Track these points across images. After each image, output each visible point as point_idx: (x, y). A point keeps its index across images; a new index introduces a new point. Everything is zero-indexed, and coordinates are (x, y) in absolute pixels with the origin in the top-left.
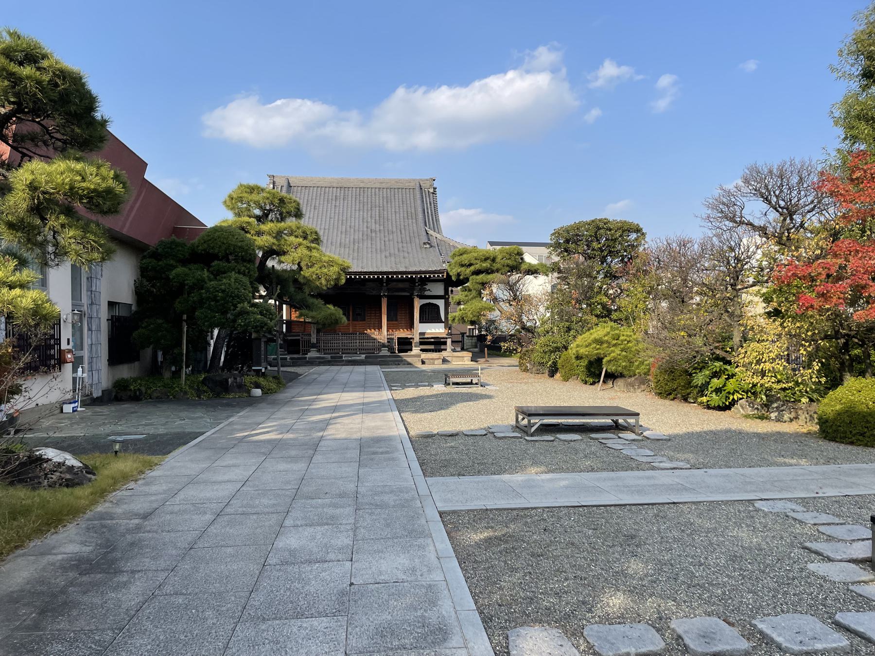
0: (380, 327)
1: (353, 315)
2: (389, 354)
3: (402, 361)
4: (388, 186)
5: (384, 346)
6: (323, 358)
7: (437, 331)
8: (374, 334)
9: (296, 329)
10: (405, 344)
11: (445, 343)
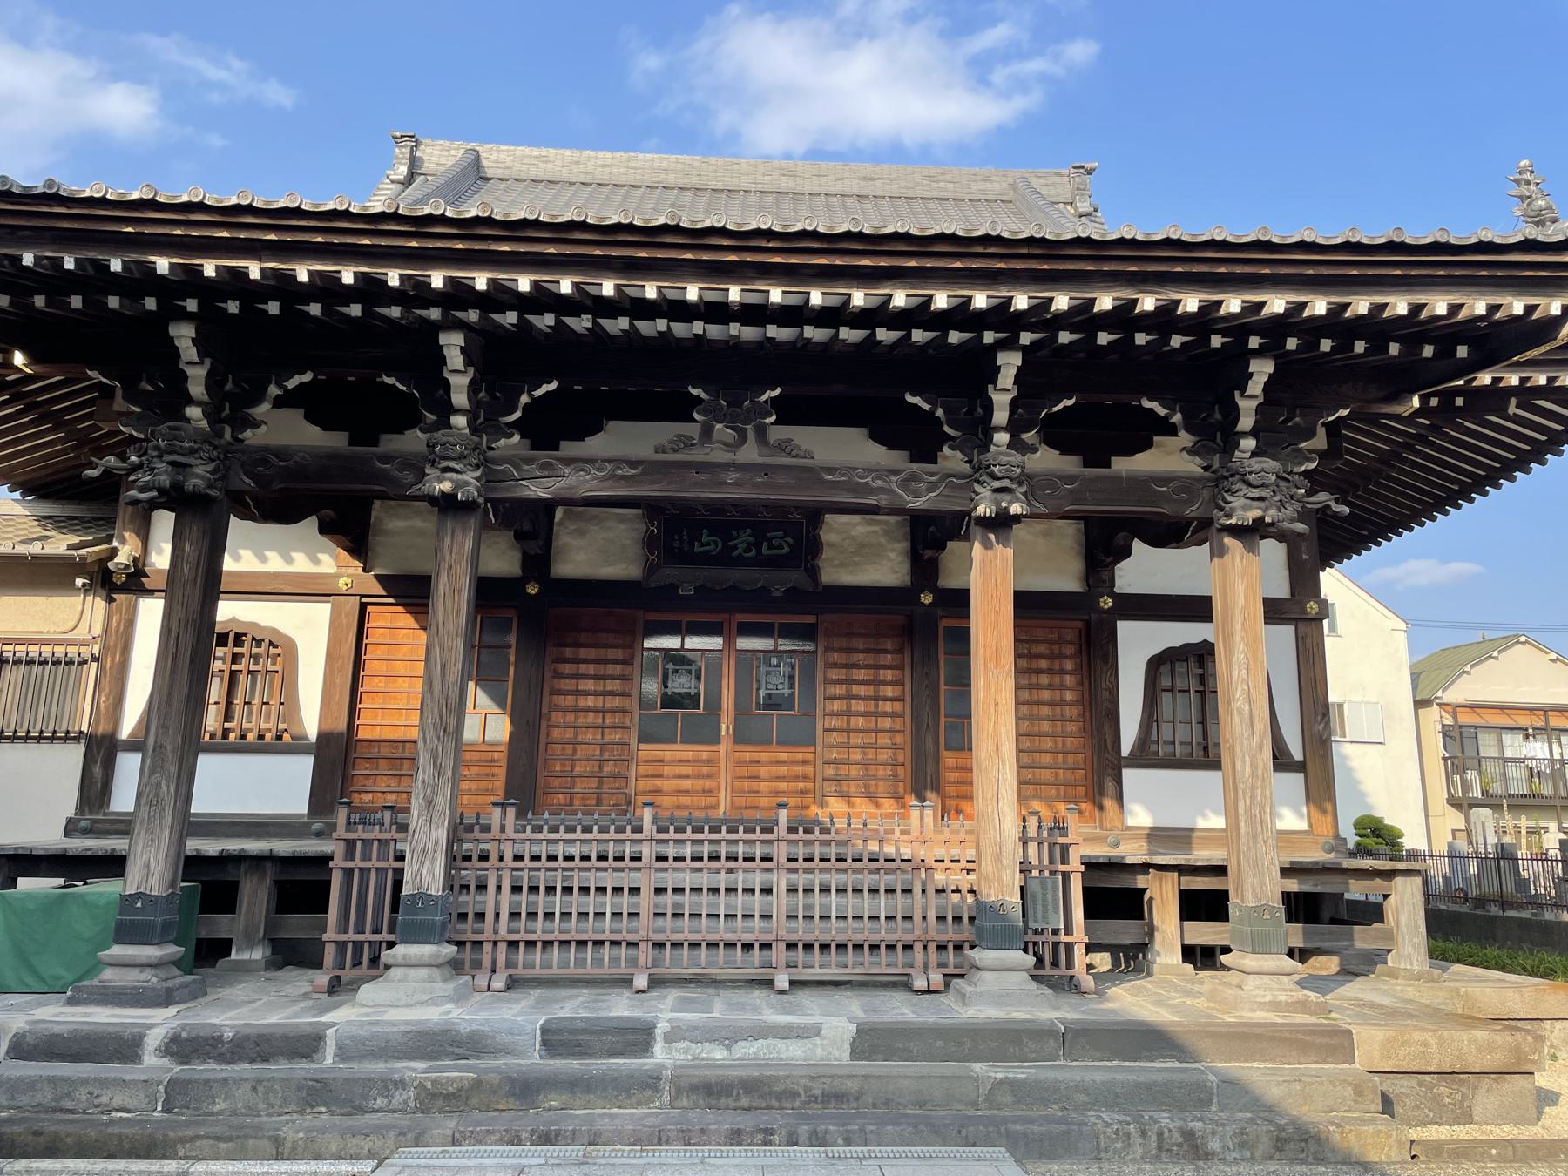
3: (1197, 1096)
5: (980, 926)
8: (914, 831)
9: (374, 789)
11: (1372, 913)
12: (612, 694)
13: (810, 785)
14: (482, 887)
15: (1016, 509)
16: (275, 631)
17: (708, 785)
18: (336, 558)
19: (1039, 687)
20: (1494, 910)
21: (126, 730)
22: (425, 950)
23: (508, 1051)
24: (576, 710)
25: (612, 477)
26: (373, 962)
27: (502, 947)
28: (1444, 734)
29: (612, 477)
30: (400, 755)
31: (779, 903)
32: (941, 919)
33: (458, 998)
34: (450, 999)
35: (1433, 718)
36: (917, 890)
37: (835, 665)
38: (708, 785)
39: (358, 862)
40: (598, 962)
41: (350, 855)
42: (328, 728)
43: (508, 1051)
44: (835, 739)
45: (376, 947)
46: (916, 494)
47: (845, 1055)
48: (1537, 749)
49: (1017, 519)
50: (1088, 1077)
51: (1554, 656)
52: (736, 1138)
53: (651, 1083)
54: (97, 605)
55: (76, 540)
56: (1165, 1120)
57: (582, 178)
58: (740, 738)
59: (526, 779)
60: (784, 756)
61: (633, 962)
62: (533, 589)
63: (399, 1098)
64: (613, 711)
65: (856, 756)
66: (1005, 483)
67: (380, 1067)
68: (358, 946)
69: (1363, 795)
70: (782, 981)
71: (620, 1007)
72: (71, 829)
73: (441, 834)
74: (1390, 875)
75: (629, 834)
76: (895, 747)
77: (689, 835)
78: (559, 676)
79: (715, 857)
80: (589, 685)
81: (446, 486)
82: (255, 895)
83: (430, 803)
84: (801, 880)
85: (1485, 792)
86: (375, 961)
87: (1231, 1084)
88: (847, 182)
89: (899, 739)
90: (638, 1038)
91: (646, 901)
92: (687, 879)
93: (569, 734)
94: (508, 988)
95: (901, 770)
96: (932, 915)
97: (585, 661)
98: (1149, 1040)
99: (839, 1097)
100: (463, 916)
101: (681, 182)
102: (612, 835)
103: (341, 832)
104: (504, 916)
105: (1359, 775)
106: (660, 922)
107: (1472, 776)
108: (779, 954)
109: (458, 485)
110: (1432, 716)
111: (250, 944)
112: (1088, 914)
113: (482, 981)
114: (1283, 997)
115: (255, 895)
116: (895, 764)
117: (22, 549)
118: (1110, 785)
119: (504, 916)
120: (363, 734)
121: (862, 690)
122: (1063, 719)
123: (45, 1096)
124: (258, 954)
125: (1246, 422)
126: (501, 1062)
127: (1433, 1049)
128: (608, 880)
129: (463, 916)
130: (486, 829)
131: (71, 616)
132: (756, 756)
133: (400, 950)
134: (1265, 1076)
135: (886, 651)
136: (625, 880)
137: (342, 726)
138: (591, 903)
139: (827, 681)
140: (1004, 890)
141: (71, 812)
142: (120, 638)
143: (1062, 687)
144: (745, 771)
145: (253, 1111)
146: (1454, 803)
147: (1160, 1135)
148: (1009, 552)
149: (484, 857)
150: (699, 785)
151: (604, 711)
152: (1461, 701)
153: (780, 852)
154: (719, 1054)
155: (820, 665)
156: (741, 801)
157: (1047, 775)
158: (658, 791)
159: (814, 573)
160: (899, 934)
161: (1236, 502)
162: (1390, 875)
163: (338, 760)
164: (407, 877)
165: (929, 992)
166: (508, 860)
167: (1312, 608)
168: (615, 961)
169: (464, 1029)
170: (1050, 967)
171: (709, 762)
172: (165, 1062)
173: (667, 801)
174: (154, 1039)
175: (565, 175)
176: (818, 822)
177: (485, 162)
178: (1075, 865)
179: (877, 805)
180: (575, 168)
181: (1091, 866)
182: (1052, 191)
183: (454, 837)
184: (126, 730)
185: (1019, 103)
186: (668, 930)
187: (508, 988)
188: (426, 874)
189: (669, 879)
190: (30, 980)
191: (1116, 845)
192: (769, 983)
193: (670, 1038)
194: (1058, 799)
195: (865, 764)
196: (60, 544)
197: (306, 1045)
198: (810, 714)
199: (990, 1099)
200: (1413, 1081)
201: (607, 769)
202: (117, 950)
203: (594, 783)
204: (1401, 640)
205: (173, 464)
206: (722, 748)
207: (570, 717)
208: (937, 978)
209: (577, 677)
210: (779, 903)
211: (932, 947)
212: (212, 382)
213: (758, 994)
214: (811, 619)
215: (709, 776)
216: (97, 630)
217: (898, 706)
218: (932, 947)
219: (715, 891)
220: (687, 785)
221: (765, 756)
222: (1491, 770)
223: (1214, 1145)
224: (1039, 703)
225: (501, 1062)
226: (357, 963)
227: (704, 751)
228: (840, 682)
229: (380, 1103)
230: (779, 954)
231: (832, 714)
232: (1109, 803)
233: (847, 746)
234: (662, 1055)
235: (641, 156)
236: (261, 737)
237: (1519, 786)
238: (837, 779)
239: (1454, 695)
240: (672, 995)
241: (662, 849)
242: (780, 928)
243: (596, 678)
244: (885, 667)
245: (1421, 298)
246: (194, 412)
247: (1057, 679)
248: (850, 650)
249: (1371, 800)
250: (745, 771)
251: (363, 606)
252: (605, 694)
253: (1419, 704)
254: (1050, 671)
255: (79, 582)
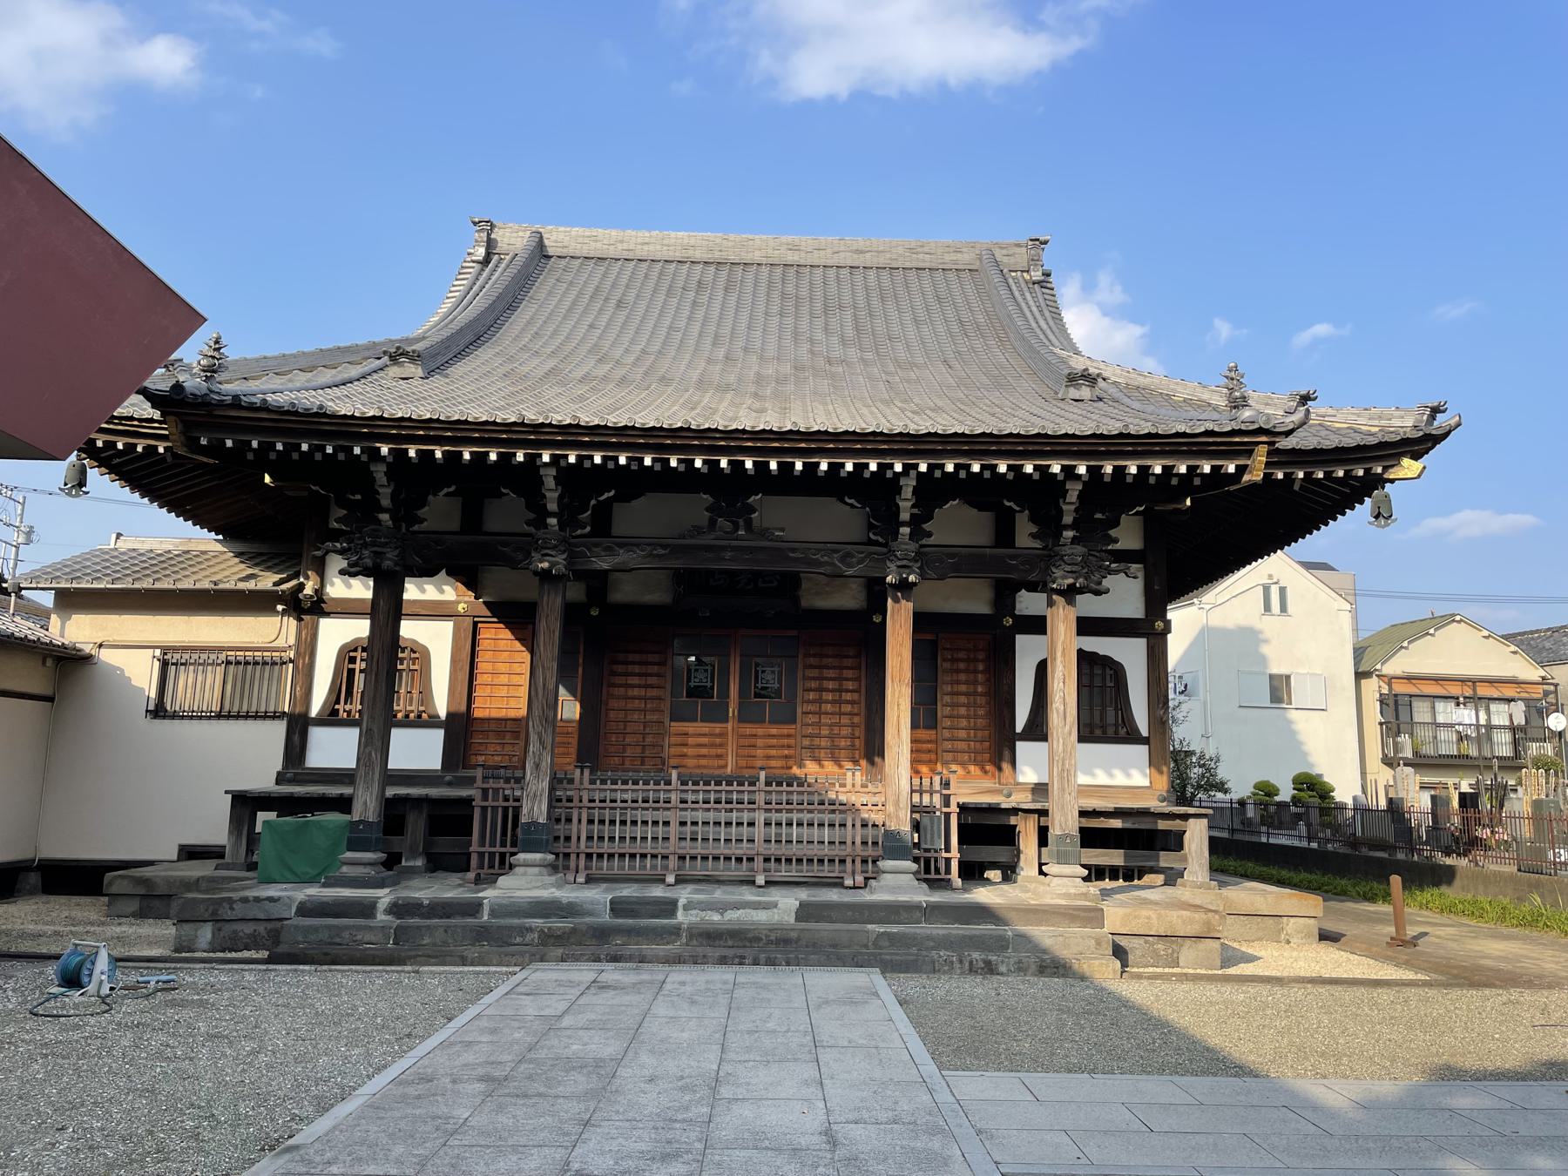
0: (872, 749)
1: (742, 694)
2: (923, 896)
3: (1001, 944)
4: (882, 261)
5: (893, 846)
6: (569, 910)
7: (1120, 779)
8: (848, 784)
9: (490, 753)
10: (989, 836)
11: (1174, 842)
12: (652, 686)
13: (792, 752)
14: (569, 820)
15: (912, 578)
16: (415, 642)
17: (719, 751)
18: (456, 589)
19: (958, 683)
20: (1365, 851)
21: (314, 711)
22: (538, 856)
23: (591, 914)
24: (626, 698)
25: (651, 555)
26: (504, 865)
27: (583, 857)
28: (1381, 702)
29: (651, 555)
30: (511, 729)
31: (759, 832)
32: (864, 843)
33: (559, 886)
34: (552, 885)
35: (1372, 687)
36: (849, 824)
37: (811, 667)
38: (719, 751)
39: (490, 803)
40: (643, 867)
41: (485, 798)
42: (453, 709)
43: (591, 914)
44: (812, 719)
45: (503, 855)
46: (850, 566)
47: (792, 920)
48: (1466, 715)
49: (914, 584)
50: (935, 932)
51: (1486, 633)
52: (723, 961)
53: (676, 931)
54: (291, 624)
55: (277, 577)
56: (976, 955)
57: (626, 255)
58: (743, 718)
59: (592, 744)
60: (774, 731)
61: (666, 868)
62: (594, 612)
63: (529, 937)
64: (652, 698)
65: (825, 732)
66: (905, 562)
67: (516, 921)
68: (492, 855)
69: (1305, 755)
70: (760, 880)
71: (657, 892)
72: (280, 779)
73: (545, 784)
74: (1185, 817)
75: (662, 786)
76: (853, 725)
77: (702, 787)
78: (613, 673)
79: (718, 802)
80: (635, 680)
81: (546, 565)
82: (416, 824)
83: (537, 766)
84: (774, 817)
85: (1416, 753)
86: (502, 862)
87: (1021, 936)
88: (842, 255)
89: (856, 720)
90: (669, 908)
91: (674, 829)
92: (700, 816)
93: (621, 715)
94: (587, 882)
95: (857, 742)
96: (858, 840)
97: (633, 663)
98: (983, 913)
99: (786, 941)
100: (557, 838)
101: (707, 257)
102: (651, 786)
103: (479, 783)
104: (583, 838)
105: (1301, 737)
106: (683, 844)
107: (1404, 739)
108: (759, 863)
109: (553, 565)
110: (1372, 687)
111: (414, 857)
112: (960, 843)
113: (570, 877)
114: (1073, 891)
115: (416, 824)
116: (853, 737)
117: (242, 586)
118: (1007, 753)
119: (583, 838)
120: (477, 714)
121: (831, 685)
122: (975, 705)
123: (324, 936)
124: (419, 862)
125: (1068, 519)
126: (588, 919)
127: (1154, 921)
128: (650, 816)
129: (557, 838)
130: (571, 781)
131: (270, 631)
132: (754, 731)
133: (522, 856)
134: (1044, 935)
135: (847, 657)
136: (661, 816)
137: (463, 708)
138: (639, 831)
139: (805, 678)
140: (902, 823)
141: (279, 768)
142: (307, 647)
143: (975, 683)
144: (746, 742)
145: (445, 943)
146: (1389, 762)
147: (971, 963)
148: (910, 605)
149: (570, 800)
150: (713, 751)
151: (645, 699)
152: (1399, 672)
153: (760, 798)
154: (716, 917)
155: (800, 666)
156: (743, 763)
157: (962, 745)
158: (684, 756)
159: (796, 600)
160: (837, 851)
161: (1058, 573)
162: (1185, 817)
163: (461, 730)
164: (525, 811)
165: (854, 888)
166: (585, 802)
167: (1159, 625)
168: (654, 867)
169: (565, 901)
170: (930, 872)
171: (720, 735)
172: (389, 918)
173: (691, 762)
174: (383, 904)
175: (612, 252)
176: (797, 778)
177: (546, 242)
178: (954, 808)
179: (822, 766)
180: (620, 246)
181: (964, 809)
182: (1012, 260)
183: (552, 789)
184: (314, 711)
185: (1075, 43)
186: (688, 848)
187: (587, 882)
188: (535, 809)
189: (689, 816)
190: (289, 876)
191: (1009, 796)
192: (753, 883)
193: (686, 908)
194: (970, 762)
195: (831, 737)
196: (267, 581)
197: (474, 908)
198: (792, 701)
199: (875, 944)
200: (1141, 940)
201: (649, 740)
202: (349, 854)
203: (639, 749)
204: (1346, 620)
205: (375, 553)
206: (730, 725)
207: (622, 704)
208: (860, 879)
209: (627, 674)
210: (759, 832)
211: (858, 861)
212: (394, 497)
213: (744, 889)
214: (795, 633)
215: (721, 745)
216: (292, 641)
217: (856, 696)
218: (858, 861)
219: (717, 824)
220: (704, 751)
221: (760, 731)
222: (1424, 734)
223: (1003, 969)
224: (958, 694)
225: (588, 919)
226: (492, 866)
227: (717, 727)
228: (814, 679)
229: (518, 940)
230: (759, 863)
231: (809, 702)
232: (1006, 766)
233: (819, 724)
234: (681, 917)
235: (673, 234)
236: (419, 716)
237: (1448, 747)
238: (811, 748)
239: (1392, 667)
240: (690, 887)
241: (684, 796)
242: (760, 847)
243: (639, 675)
244: (847, 668)
245: (1148, 462)
246: (385, 517)
247: (972, 677)
248: (822, 656)
249: (1311, 759)
250: (746, 742)
251: (475, 624)
252: (647, 686)
253: (1360, 675)
254: (966, 671)
255: (280, 608)
